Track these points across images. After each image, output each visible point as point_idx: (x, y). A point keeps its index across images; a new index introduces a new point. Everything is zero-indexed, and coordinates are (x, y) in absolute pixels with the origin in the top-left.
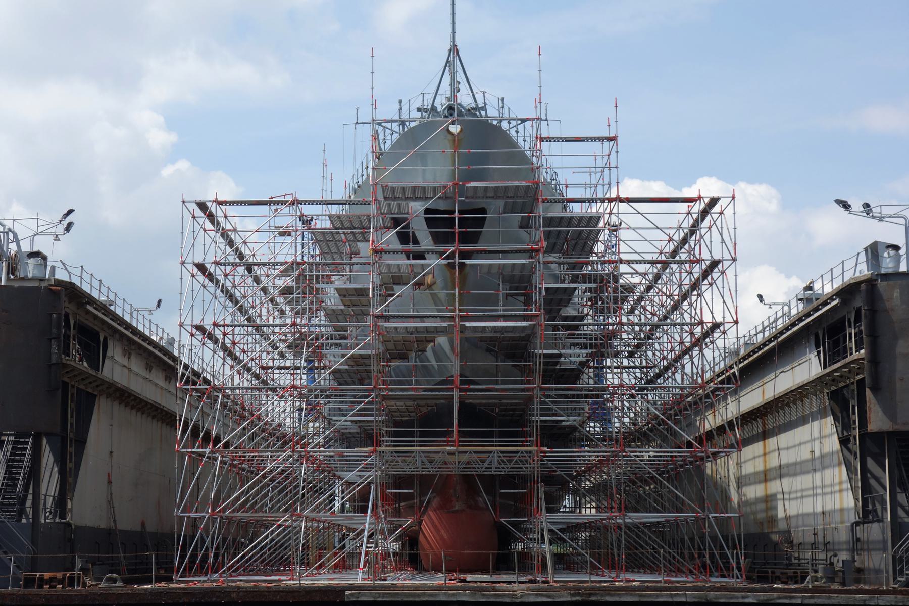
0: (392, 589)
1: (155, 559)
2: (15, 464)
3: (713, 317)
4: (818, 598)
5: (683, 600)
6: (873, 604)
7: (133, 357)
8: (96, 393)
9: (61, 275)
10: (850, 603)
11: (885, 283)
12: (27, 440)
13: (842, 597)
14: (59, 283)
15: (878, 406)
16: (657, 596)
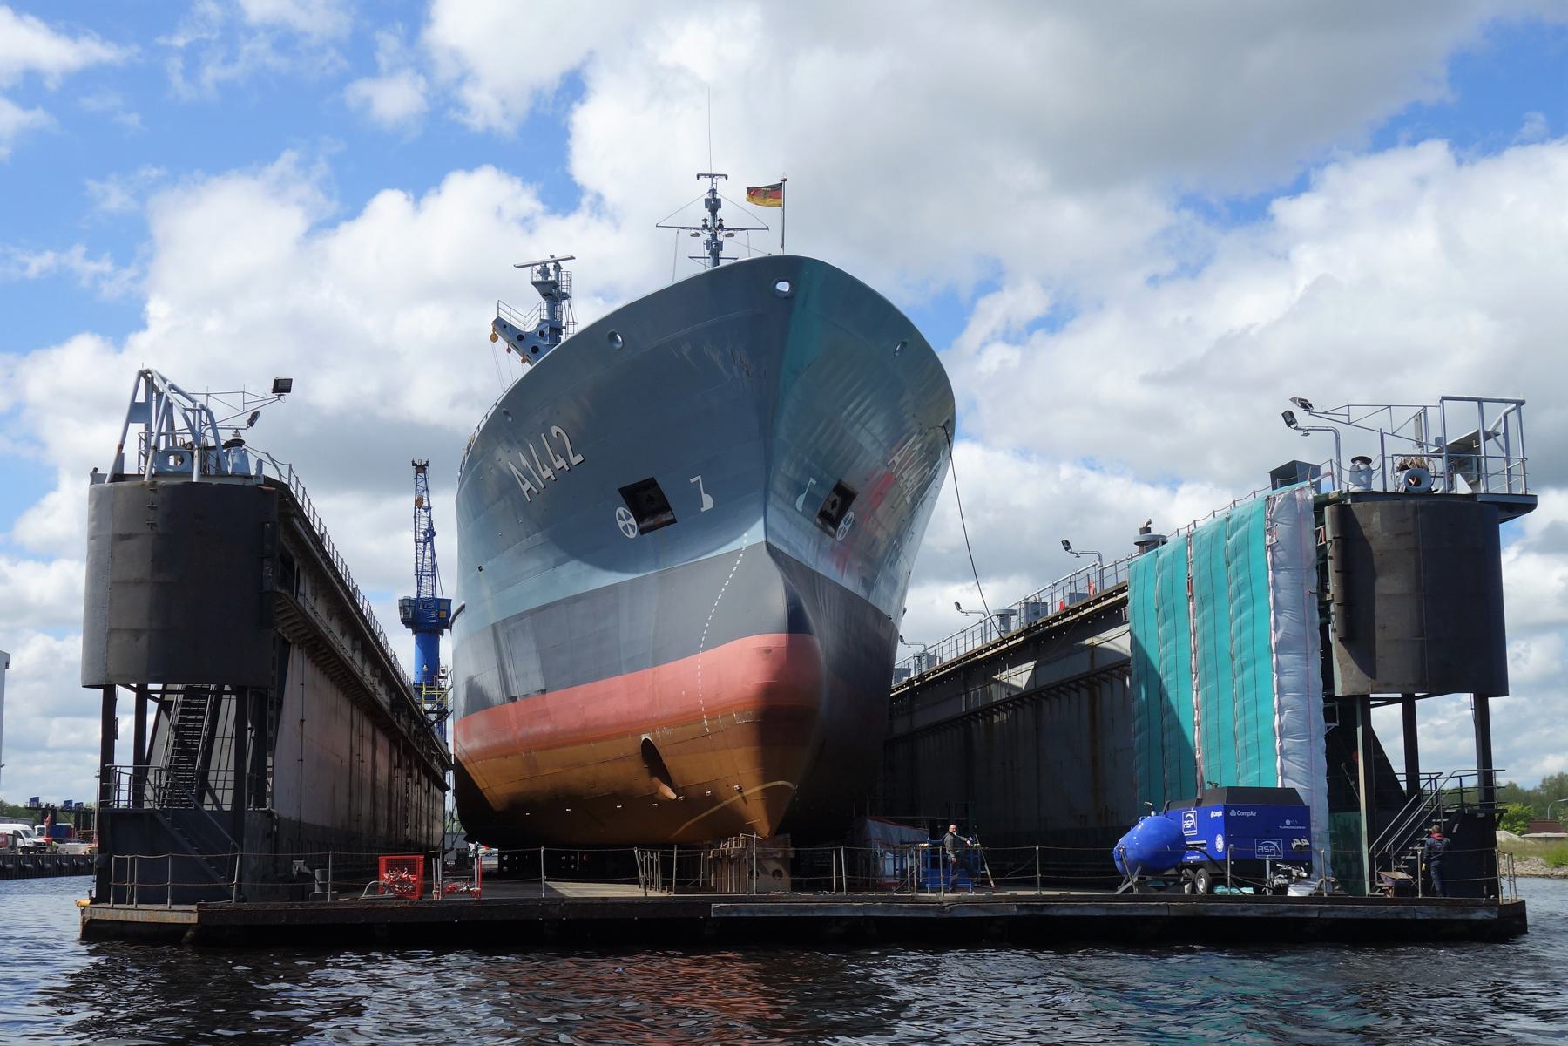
0: (774, 900)
1: (332, 862)
2: (189, 733)
3: (1492, 475)
4: (1340, 909)
5: (1165, 913)
6: (1409, 917)
7: (318, 600)
8: (290, 640)
9: (269, 472)
10: (1380, 917)
11: (1359, 505)
12: (203, 701)
13: (1369, 909)
14: (269, 481)
15: (1353, 661)
16: (1131, 908)
